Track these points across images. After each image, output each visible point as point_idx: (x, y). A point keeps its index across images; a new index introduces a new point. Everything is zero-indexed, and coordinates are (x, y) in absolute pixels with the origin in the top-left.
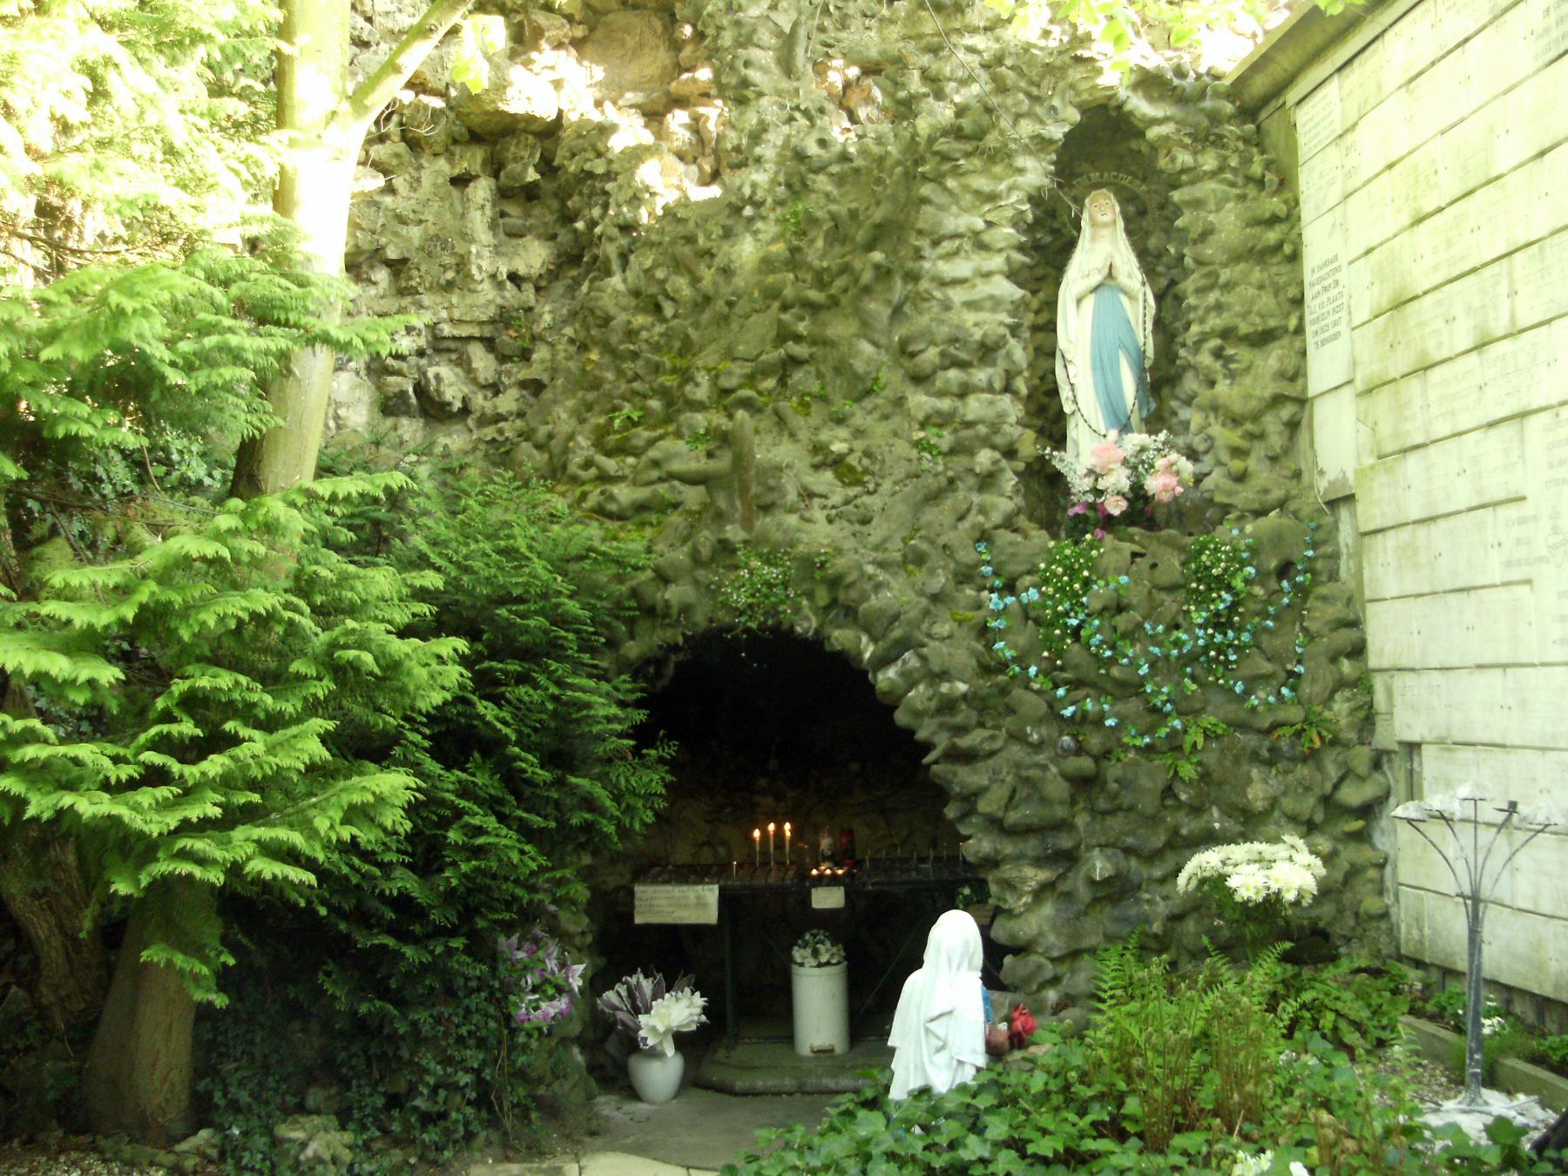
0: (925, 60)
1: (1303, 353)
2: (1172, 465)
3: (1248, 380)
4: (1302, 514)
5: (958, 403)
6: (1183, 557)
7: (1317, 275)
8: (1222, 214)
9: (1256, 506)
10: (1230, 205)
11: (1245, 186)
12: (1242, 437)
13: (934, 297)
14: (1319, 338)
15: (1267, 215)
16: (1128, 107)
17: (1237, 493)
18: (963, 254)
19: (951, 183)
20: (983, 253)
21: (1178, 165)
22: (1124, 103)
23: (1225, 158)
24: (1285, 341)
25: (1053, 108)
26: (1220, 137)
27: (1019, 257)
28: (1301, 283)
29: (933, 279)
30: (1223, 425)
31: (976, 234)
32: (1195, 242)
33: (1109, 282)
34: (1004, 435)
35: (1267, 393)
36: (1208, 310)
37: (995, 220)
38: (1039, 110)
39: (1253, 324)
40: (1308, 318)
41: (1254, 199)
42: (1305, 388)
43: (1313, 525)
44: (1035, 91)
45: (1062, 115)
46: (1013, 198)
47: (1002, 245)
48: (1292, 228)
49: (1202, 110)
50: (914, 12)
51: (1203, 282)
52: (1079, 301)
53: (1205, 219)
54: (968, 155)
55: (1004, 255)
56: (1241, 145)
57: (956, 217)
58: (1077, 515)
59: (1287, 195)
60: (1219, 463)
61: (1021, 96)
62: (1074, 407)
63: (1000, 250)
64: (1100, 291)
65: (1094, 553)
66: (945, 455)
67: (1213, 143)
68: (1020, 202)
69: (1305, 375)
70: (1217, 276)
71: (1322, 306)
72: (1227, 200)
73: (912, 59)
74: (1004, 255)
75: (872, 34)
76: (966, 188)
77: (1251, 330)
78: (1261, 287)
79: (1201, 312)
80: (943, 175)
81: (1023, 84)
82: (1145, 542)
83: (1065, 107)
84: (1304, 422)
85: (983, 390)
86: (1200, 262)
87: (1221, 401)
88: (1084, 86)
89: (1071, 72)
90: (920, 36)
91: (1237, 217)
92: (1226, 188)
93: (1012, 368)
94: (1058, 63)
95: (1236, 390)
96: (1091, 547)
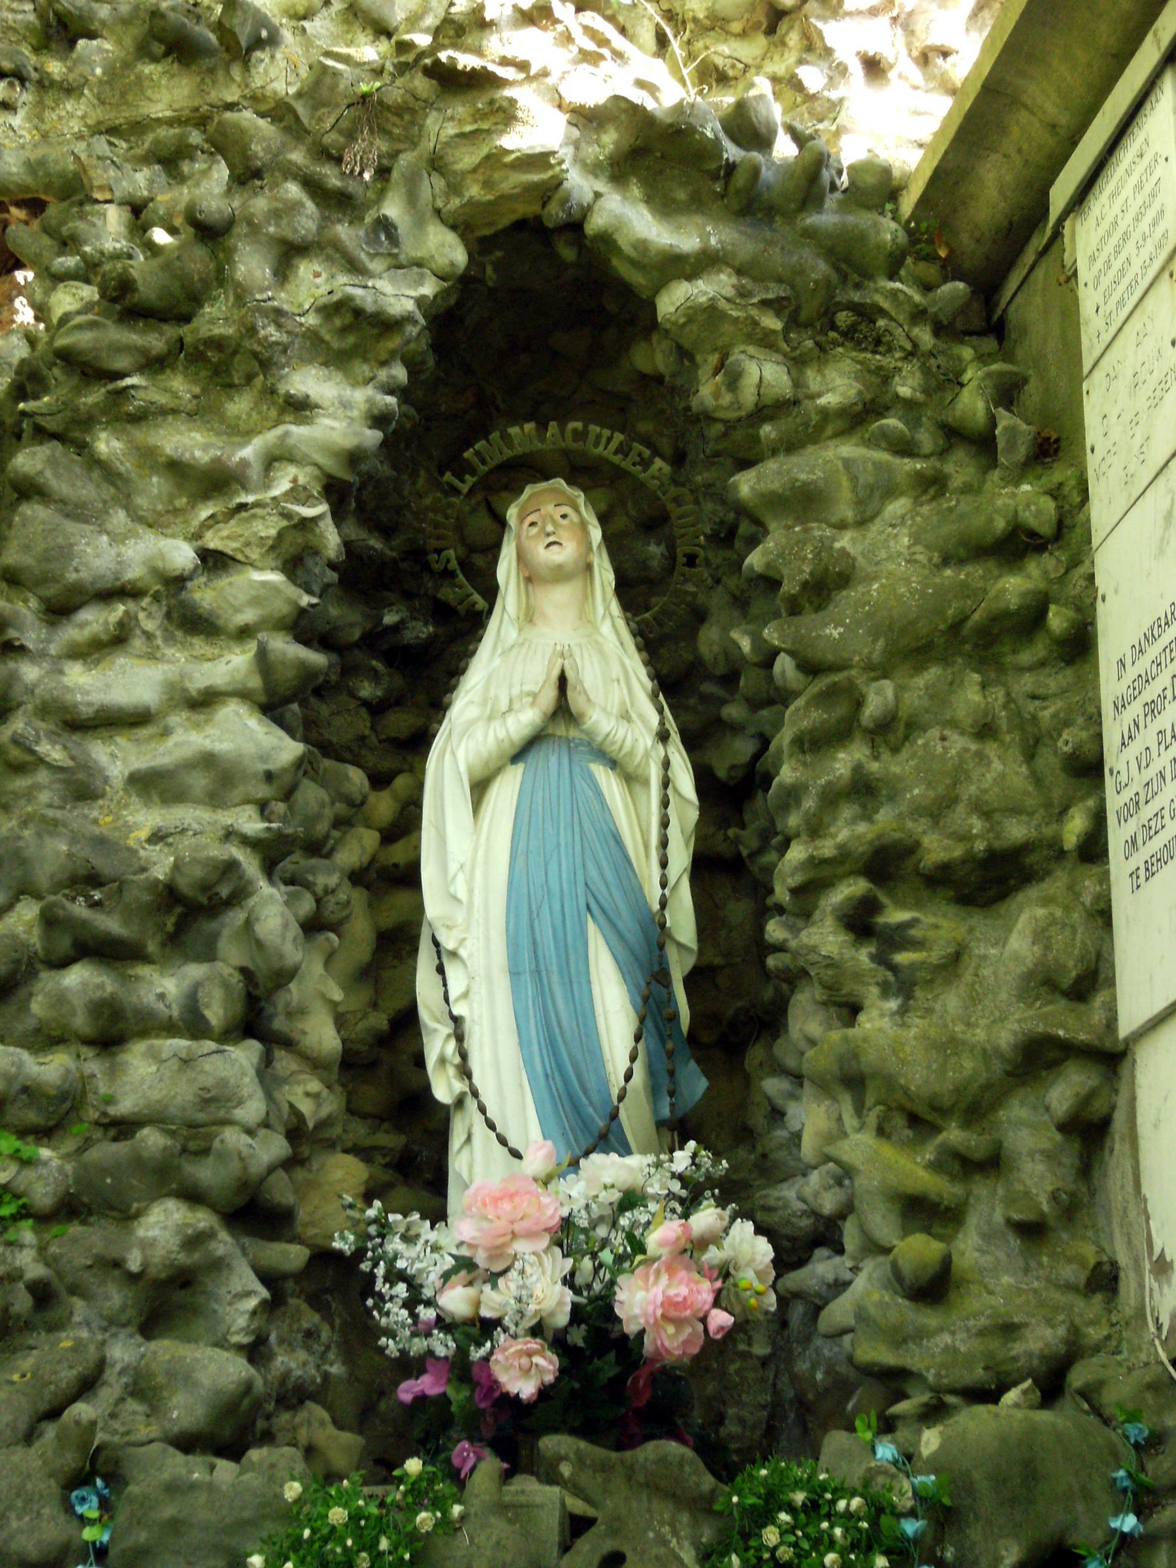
0: (141, 181)
1: (1103, 915)
2: (701, 1244)
3: (951, 1001)
4: (1109, 1397)
5: (94, 1066)
6: (707, 1535)
7: (1132, 673)
8: (875, 528)
9: (977, 1374)
10: (897, 507)
11: (943, 453)
12: (936, 1166)
13: (41, 761)
14: (1138, 859)
15: (1000, 524)
16: (597, 222)
17: (920, 1335)
18: (138, 643)
19: (106, 444)
20: (199, 644)
21: (748, 396)
22: (586, 211)
23: (885, 377)
24: (1056, 884)
25: (385, 226)
26: (867, 313)
27: (286, 648)
28: (1095, 720)
29: (45, 710)
30: (881, 1132)
31: (177, 582)
32: (794, 608)
33: (560, 730)
34: (223, 1157)
35: (1006, 1037)
36: (832, 798)
37: (228, 547)
38: (343, 231)
39: (964, 837)
40: (1114, 802)
41: (967, 489)
42: (1111, 1023)
43: (1137, 1431)
44: (332, 177)
45: (410, 249)
46: (282, 486)
47: (248, 616)
48: (1075, 563)
49: (810, 234)
50: (127, 65)
51: (816, 716)
52: (480, 788)
53: (823, 547)
54: (154, 365)
55: (252, 646)
56: (925, 336)
57: (117, 539)
58: (421, 1399)
59: (1060, 473)
60: (875, 1248)
61: (293, 190)
62: (459, 1086)
63: (244, 633)
64: (536, 757)
65: (425, 1519)
66: (42, 1219)
67: (849, 335)
68: (297, 493)
69: (1111, 982)
70: (859, 703)
71: (1143, 763)
72: (890, 492)
73: (100, 175)
74: (252, 646)
75: (17, 120)
76: (148, 457)
77: (958, 852)
78: (985, 731)
79: (809, 803)
80: (87, 422)
81: (297, 156)
82: (586, 1479)
83: (419, 224)
84: (1119, 1118)
85: (170, 1029)
86: (811, 668)
87: (870, 1058)
88: (466, 159)
89: (432, 121)
90: (139, 127)
91: (916, 539)
92: (883, 456)
93: (261, 967)
94: (395, 94)
95: (917, 1024)
96: (419, 1495)
